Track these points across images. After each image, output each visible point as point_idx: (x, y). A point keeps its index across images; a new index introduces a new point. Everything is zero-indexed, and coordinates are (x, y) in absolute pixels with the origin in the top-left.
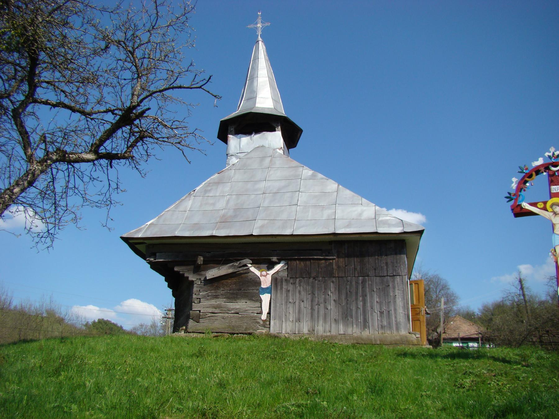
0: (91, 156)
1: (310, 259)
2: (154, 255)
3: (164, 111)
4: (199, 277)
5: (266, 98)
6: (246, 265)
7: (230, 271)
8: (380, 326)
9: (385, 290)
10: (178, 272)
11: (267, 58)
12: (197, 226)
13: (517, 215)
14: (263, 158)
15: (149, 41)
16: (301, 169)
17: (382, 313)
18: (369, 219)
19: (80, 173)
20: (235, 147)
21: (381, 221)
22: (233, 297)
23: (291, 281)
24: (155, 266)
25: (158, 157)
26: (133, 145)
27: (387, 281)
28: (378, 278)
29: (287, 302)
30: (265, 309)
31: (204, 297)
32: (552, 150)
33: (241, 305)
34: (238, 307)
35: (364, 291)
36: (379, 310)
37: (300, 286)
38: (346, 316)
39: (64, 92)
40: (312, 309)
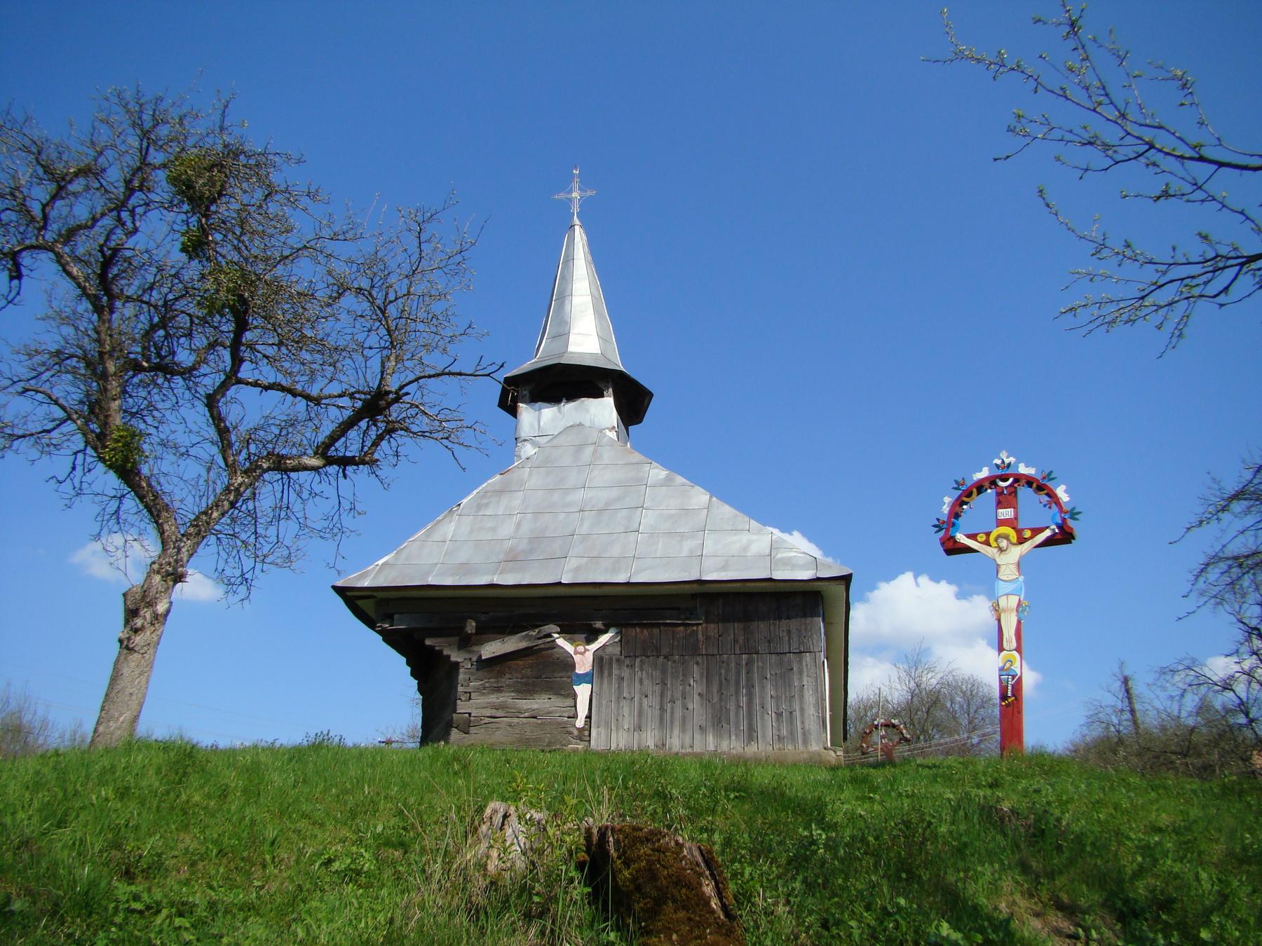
0: (315, 462)
1: (659, 625)
2: (389, 617)
3: (425, 392)
4: (467, 656)
5: (586, 337)
6: (549, 635)
7: (523, 645)
8: (776, 737)
9: (784, 677)
10: (432, 647)
11: (590, 258)
12: (465, 567)
14: (580, 448)
15: (409, 293)
16: (647, 467)
17: (779, 715)
18: (760, 556)
19: (297, 487)
20: (531, 425)
21: (781, 559)
22: (528, 689)
23: (627, 661)
24: (392, 639)
25: (410, 459)
26: (376, 444)
27: (790, 662)
28: (774, 656)
29: (620, 697)
30: (582, 710)
31: (478, 690)
32: (1004, 455)
33: (540, 702)
34: (535, 706)
36: (774, 709)
37: (642, 670)
38: (719, 721)
39: (267, 357)
40: (662, 709)
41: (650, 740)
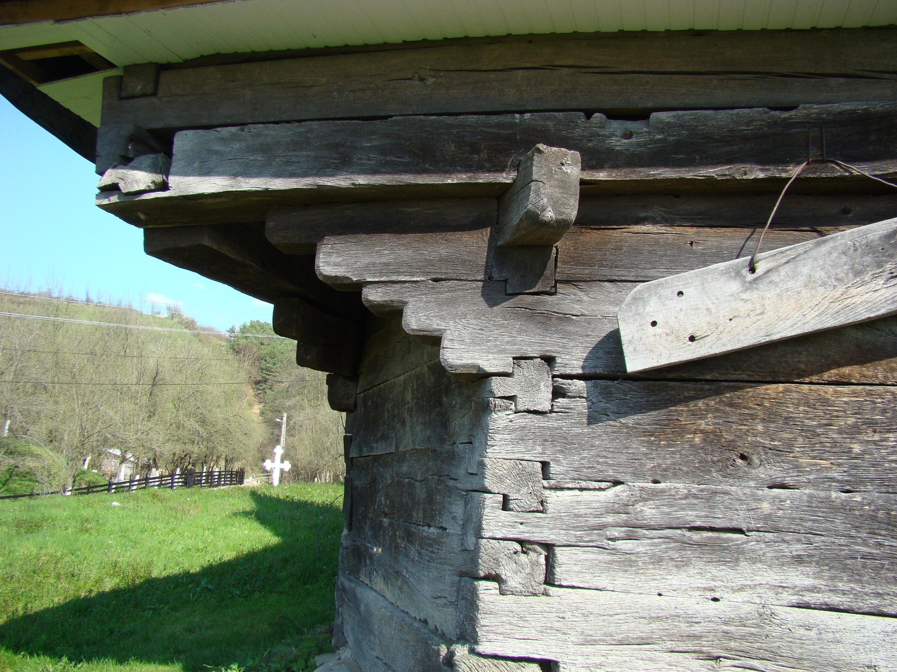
4: (533, 342)
10: (349, 292)
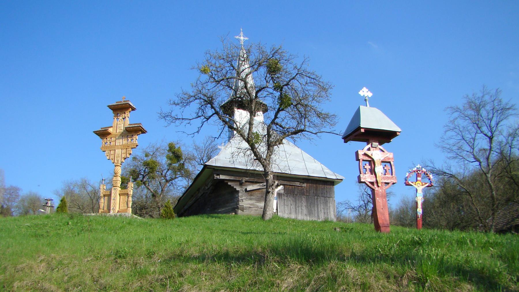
7: (259, 187)
9: (326, 203)
13: (406, 185)
17: (325, 213)
35: (317, 203)
40: (296, 209)
41: (293, 216)
